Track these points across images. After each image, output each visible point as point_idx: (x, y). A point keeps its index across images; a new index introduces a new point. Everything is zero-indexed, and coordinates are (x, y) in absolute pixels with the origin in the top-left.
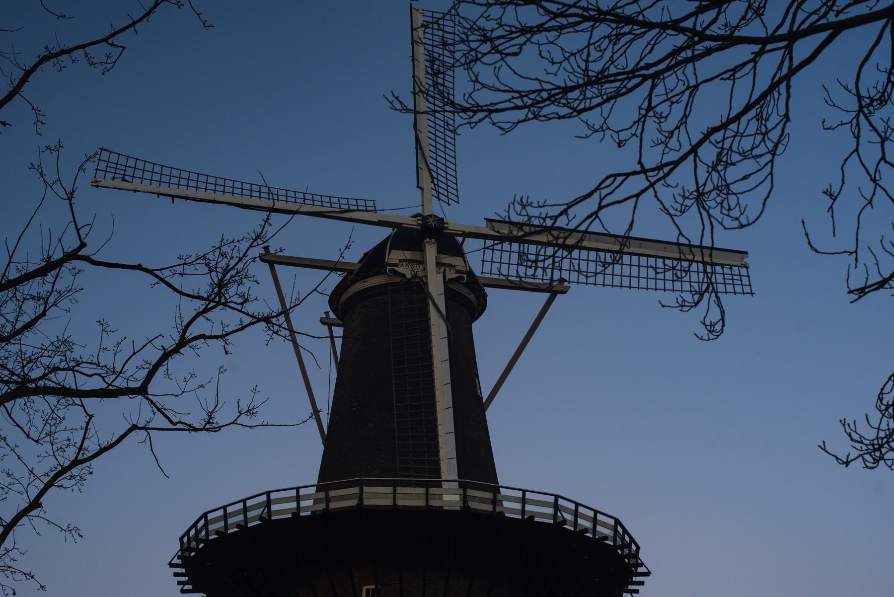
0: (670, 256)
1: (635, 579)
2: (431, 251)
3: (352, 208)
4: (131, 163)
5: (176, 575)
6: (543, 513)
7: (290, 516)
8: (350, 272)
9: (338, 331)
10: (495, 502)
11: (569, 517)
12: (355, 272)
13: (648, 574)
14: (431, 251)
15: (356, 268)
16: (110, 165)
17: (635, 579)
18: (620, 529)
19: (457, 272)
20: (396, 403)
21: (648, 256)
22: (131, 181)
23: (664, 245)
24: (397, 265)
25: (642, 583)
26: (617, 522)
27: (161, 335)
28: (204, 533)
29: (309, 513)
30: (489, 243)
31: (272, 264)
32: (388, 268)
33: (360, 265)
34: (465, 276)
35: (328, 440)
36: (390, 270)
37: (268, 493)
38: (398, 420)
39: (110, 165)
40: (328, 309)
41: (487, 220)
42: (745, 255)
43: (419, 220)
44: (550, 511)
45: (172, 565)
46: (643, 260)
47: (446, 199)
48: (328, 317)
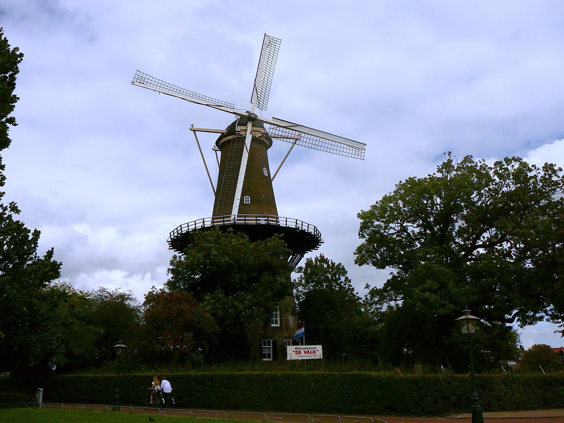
0: (337, 141)
1: (319, 244)
2: (250, 125)
3: (222, 105)
4: (353, 156)
5: (169, 244)
6: (292, 225)
7: (201, 227)
8: (223, 134)
9: (219, 153)
10: (277, 222)
11: (300, 226)
12: (225, 134)
13: (323, 243)
14: (250, 125)
15: (225, 132)
16: (139, 77)
17: (319, 244)
18: (316, 229)
19: (262, 133)
20: (266, 358)
21: (311, 135)
22: (146, 84)
23: (352, 141)
24: (240, 132)
25: (321, 245)
26: (315, 227)
27: (251, 102)
28: (180, 231)
29: (185, 232)
30: (272, 126)
31: (194, 131)
32: (237, 133)
33: (226, 131)
34: (264, 135)
35: (217, 194)
36: (238, 133)
37: (204, 219)
38: (267, 358)
39: (360, 155)
40: (215, 145)
41: (273, 118)
42: (365, 145)
43: (248, 114)
44: (295, 224)
45: (168, 242)
46: (339, 145)
47: (261, 108)
48: (215, 148)
